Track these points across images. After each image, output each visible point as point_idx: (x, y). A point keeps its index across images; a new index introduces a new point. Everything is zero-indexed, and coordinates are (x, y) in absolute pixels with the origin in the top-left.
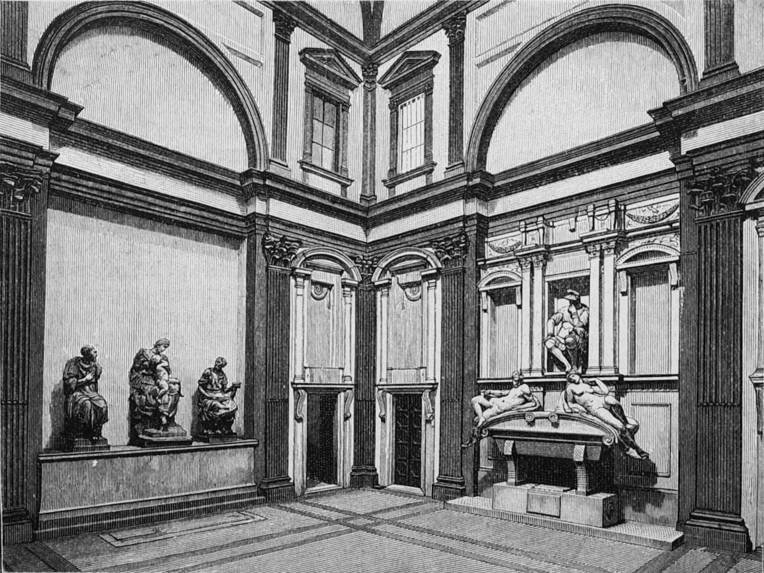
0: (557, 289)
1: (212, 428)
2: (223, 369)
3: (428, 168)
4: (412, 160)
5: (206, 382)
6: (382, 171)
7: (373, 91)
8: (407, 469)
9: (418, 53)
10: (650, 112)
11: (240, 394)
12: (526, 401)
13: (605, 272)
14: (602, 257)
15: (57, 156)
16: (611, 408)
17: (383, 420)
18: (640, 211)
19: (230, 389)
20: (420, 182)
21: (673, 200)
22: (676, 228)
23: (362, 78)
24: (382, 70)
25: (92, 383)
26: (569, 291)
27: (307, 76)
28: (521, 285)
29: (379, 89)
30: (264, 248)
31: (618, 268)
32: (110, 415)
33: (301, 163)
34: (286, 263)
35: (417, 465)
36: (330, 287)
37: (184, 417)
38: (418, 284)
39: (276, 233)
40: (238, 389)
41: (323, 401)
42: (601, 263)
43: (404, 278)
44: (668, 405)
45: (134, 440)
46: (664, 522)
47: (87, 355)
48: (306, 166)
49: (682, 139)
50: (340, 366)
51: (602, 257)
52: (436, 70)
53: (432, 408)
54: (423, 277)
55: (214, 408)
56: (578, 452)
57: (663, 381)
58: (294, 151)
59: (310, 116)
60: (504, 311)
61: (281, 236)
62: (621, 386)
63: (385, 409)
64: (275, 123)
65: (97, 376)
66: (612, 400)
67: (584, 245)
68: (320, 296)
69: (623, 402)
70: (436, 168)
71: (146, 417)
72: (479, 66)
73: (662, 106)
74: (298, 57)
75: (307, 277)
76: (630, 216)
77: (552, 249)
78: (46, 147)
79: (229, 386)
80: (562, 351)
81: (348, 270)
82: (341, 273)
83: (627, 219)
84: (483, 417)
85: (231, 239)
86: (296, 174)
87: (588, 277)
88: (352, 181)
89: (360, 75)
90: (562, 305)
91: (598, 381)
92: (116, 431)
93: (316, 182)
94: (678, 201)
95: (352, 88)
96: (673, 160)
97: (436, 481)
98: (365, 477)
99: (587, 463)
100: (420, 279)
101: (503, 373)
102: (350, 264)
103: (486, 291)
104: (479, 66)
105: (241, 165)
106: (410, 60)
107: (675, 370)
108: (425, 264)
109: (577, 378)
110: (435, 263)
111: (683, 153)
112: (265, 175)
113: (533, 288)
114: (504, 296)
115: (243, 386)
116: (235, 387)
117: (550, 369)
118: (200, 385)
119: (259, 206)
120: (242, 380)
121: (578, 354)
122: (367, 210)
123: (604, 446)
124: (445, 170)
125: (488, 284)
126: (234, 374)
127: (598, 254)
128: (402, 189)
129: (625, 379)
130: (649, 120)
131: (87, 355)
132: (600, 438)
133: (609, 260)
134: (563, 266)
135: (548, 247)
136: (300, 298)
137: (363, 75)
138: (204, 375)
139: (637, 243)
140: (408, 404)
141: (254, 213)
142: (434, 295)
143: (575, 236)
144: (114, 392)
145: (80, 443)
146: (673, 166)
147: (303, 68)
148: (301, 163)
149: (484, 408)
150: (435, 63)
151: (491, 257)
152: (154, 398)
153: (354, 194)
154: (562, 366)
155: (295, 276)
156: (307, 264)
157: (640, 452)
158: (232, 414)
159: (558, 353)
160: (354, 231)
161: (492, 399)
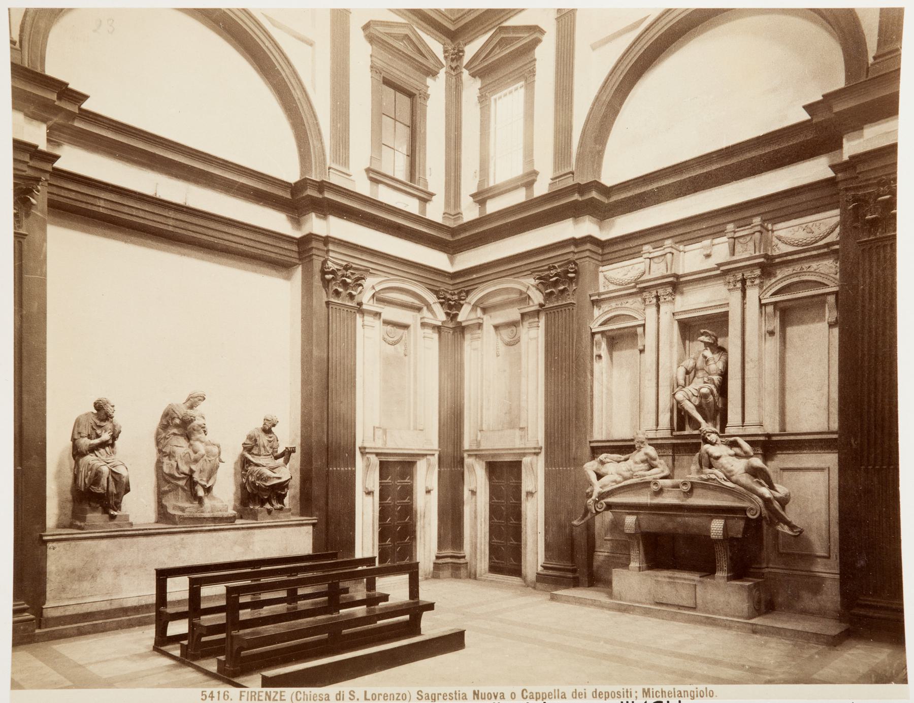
0: (688, 328)
1: (257, 496)
2: (273, 429)
3: (529, 181)
4: (507, 168)
5: (251, 446)
6: (469, 186)
7: (459, 76)
8: (506, 558)
9: (515, 29)
10: (805, 107)
11: (296, 459)
12: (652, 467)
13: (747, 310)
14: (744, 291)
15: (57, 157)
16: (754, 472)
17: (473, 493)
18: (790, 233)
19: (282, 455)
20: (519, 197)
21: (830, 218)
22: (836, 251)
23: (444, 62)
24: (470, 50)
25: (108, 445)
26: (702, 331)
27: (374, 59)
28: (644, 325)
29: (466, 74)
30: (323, 279)
31: (763, 302)
32: (132, 487)
33: (368, 170)
34: (351, 297)
35: (517, 552)
36: (406, 327)
37: (224, 494)
38: (514, 324)
39: (336, 259)
40: (293, 455)
41: (397, 470)
42: (744, 297)
43: (501, 317)
44: (822, 469)
45: (163, 515)
46: (820, 613)
47: (102, 412)
48: (376, 177)
49: (844, 140)
50: (420, 435)
51: (744, 291)
52: (539, 51)
53: (534, 479)
54: (523, 315)
55: (260, 477)
56: (717, 527)
57: (821, 440)
58: (360, 154)
59: (378, 114)
60: (625, 355)
61: (344, 264)
62: (768, 446)
63: (477, 480)
64: (334, 121)
65: (114, 437)
66: (757, 462)
67: (724, 273)
68: (395, 339)
69: (772, 467)
70: (539, 178)
71: (181, 486)
72: (594, 47)
73: (821, 98)
74: (362, 33)
75: (377, 314)
76: (779, 238)
77: (682, 280)
78: (43, 146)
79: (280, 450)
80: (696, 406)
81: (429, 306)
82: (419, 309)
83: (776, 241)
84: (597, 487)
85: (281, 266)
86: (363, 187)
87: (726, 314)
88: (432, 195)
89: (441, 56)
90: (698, 347)
91: (741, 441)
92: (139, 506)
93: (385, 195)
94: (838, 219)
95: (433, 74)
96: (832, 167)
97: (540, 568)
98: (452, 565)
99: (728, 539)
100: (518, 317)
101: (621, 431)
102: (431, 298)
103: (603, 333)
104: (594, 47)
105: (292, 175)
106: (503, 38)
107: (835, 426)
108: (525, 298)
109: (713, 438)
110: (537, 298)
111: (846, 157)
112: (322, 186)
113: (659, 323)
114: (620, 338)
115: (298, 450)
116: (287, 454)
117: (681, 427)
118: (245, 448)
119: (316, 225)
120: (297, 444)
121: (716, 409)
122: (453, 231)
123: (748, 519)
124: (550, 181)
125: (604, 323)
126: (288, 434)
127: (739, 285)
128: (493, 206)
129: (774, 438)
130: (805, 116)
131: (102, 412)
132: (743, 510)
133: (753, 294)
134: (697, 301)
135: (677, 276)
136: (369, 340)
137: (446, 58)
138: (250, 438)
139: (788, 271)
140: (504, 472)
141: (311, 234)
142: (534, 337)
143: (711, 263)
144: (134, 458)
145: (95, 517)
146: (833, 175)
147: (367, 48)
148: (368, 170)
149: (599, 476)
150: (537, 41)
151: (606, 290)
152: (187, 463)
153: (435, 212)
154: (696, 425)
155: (362, 312)
156: (378, 298)
157: (792, 527)
158: (283, 486)
159: (690, 408)
160: (437, 259)
161: (607, 465)
